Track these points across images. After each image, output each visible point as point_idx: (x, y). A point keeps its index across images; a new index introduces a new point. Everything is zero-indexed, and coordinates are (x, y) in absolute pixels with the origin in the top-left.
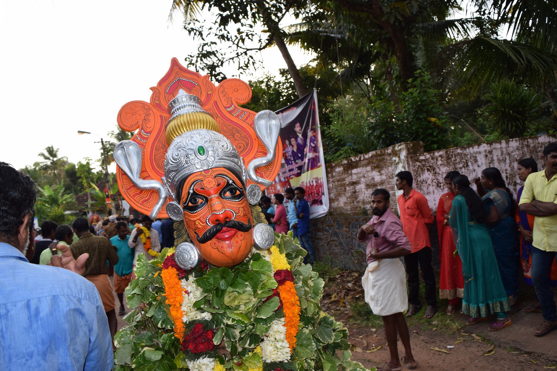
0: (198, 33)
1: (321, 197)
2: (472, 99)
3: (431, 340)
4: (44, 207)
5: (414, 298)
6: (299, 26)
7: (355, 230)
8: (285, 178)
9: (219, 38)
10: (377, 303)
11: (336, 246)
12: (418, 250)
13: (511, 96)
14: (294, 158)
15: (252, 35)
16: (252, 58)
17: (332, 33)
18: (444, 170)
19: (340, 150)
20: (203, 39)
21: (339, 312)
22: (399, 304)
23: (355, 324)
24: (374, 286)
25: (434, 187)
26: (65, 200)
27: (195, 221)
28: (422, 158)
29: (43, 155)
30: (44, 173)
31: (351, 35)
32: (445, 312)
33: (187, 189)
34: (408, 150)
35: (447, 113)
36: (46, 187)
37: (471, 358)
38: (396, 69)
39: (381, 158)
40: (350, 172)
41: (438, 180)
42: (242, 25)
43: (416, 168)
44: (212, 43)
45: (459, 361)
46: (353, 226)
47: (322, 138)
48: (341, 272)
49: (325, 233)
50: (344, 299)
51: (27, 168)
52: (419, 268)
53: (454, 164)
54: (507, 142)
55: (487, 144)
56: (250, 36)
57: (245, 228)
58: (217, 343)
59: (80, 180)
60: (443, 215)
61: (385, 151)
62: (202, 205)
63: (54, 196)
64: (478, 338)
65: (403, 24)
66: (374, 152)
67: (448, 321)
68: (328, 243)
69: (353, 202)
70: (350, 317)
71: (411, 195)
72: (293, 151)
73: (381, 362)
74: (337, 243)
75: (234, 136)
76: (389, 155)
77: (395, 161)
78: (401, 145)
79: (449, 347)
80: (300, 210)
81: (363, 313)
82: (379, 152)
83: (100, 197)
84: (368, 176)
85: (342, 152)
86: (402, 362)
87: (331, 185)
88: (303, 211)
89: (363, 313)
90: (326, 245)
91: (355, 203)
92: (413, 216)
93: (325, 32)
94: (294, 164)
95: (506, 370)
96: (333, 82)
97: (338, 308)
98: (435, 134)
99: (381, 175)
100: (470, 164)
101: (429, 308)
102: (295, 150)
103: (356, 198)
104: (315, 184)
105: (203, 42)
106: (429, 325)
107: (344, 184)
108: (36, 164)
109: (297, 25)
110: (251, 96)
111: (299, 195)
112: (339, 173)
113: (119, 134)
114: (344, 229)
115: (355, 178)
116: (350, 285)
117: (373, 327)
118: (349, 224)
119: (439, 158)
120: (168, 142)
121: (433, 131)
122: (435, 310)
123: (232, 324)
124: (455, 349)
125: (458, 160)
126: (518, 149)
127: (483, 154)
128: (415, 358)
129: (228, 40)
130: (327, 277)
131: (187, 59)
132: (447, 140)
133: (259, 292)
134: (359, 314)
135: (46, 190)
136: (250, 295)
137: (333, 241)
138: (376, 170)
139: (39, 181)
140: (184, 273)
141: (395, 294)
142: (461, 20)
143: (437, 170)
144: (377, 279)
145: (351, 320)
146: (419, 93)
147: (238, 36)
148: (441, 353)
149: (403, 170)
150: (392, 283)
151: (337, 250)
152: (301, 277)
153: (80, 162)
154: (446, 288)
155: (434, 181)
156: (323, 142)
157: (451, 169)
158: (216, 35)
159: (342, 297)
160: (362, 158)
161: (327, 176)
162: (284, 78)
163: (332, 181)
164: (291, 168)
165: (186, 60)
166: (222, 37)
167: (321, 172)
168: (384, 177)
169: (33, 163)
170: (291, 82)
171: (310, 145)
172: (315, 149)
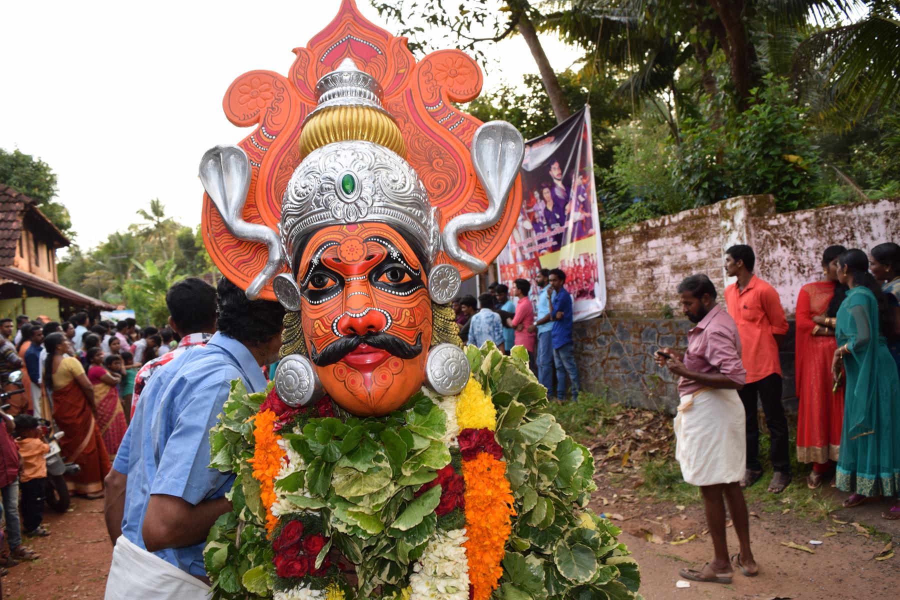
0: (393, 13)
1: (593, 285)
2: (849, 127)
3: (782, 529)
4: (145, 295)
7: (650, 342)
8: (531, 254)
9: (428, 20)
10: (689, 464)
11: (617, 368)
12: (758, 379)
14: (547, 221)
15: (483, 15)
16: (482, 54)
17: (612, 15)
19: (629, 207)
20: (402, 22)
21: (621, 476)
22: (730, 468)
23: (649, 496)
24: (686, 436)
25: (793, 273)
28: (773, 222)
29: (143, 213)
30: (143, 242)
31: (648, 16)
32: (804, 482)
34: (749, 208)
37: (852, 563)
39: (699, 222)
40: (644, 245)
41: (799, 260)
43: (761, 240)
44: (417, 29)
45: (832, 567)
46: (647, 335)
47: (597, 189)
48: (623, 411)
49: (599, 346)
50: (630, 454)
51: (118, 233)
52: (760, 408)
53: (830, 234)
55: (890, 201)
56: (480, 18)
57: (407, 351)
59: (200, 253)
60: (811, 318)
61: (707, 210)
63: (159, 278)
64: (863, 529)
67: (810, 499)
68: (603, 363)
69: (648, 296)
70: (640, 485)
71: (750, 285)
72: (546, 210)
73: (696, 561)
74: (618, 363)
75: (431, 163)
76: (715, 217)
77: (725, 227)
78: (736, 200)
79: (812, 542)
80: (556, 307)
81: (662, 479)
82: (696, 212)
84: (676, 253)
85: (632, 211)
86: (733, 563)
87: (610, 267)
88: (563, 308)
89: (662, 479)
90: (599, 364)
91: (652, 298)
92: (753, 321)
93: (601, 12)
94: (547, 230)
96: (612, 97)
97: (620, 470)
98: (795, 182)
100: (857, 234)
101: (776, 475)
102: (550, 208)
103: (654, 288)
104: (583, 264)
106: (775, 503)
107: (634, 265)
108: (133, 227)
111: (556, 283)
112: (626, 247)
114: (632, 339)
115: (652, 255)
116: (639, 432)
117: (679, 502)
118: (641, 332)
119: (804, 224)
121: (793, 178)
122: (786, 479)
124: (824, 546)
125: (837, 228)
127: (882, 218)
128: (755, 559)
129: (444, 23)
130: (602, 417)
132: (815, 194)
134: (656, 480)
135: (148, 268)
137: (611, 359)
138: (691, 242)
139: (136, 253)
143: (799, 244)
144: (689, 424)
145: (642, 490)
146: (770, 113)
147: (461, 18)
148: (799, 552)
149: (739, 243)
150: (712, 433)
151: (618, 374)
154: (815, 445)
156: (598, 195)
158: (424, 16)
159: (627, 451)
160: (667, 223)
161: (604, 252)
162: (531, 89)
163: (614, 260)
164: (541, 238)
166: (434, 19)
167: (593, 244)
168: (704, 255)
169: (128, 226)
170: (542, 97)
171: (577, 200)
172: (585, 206)
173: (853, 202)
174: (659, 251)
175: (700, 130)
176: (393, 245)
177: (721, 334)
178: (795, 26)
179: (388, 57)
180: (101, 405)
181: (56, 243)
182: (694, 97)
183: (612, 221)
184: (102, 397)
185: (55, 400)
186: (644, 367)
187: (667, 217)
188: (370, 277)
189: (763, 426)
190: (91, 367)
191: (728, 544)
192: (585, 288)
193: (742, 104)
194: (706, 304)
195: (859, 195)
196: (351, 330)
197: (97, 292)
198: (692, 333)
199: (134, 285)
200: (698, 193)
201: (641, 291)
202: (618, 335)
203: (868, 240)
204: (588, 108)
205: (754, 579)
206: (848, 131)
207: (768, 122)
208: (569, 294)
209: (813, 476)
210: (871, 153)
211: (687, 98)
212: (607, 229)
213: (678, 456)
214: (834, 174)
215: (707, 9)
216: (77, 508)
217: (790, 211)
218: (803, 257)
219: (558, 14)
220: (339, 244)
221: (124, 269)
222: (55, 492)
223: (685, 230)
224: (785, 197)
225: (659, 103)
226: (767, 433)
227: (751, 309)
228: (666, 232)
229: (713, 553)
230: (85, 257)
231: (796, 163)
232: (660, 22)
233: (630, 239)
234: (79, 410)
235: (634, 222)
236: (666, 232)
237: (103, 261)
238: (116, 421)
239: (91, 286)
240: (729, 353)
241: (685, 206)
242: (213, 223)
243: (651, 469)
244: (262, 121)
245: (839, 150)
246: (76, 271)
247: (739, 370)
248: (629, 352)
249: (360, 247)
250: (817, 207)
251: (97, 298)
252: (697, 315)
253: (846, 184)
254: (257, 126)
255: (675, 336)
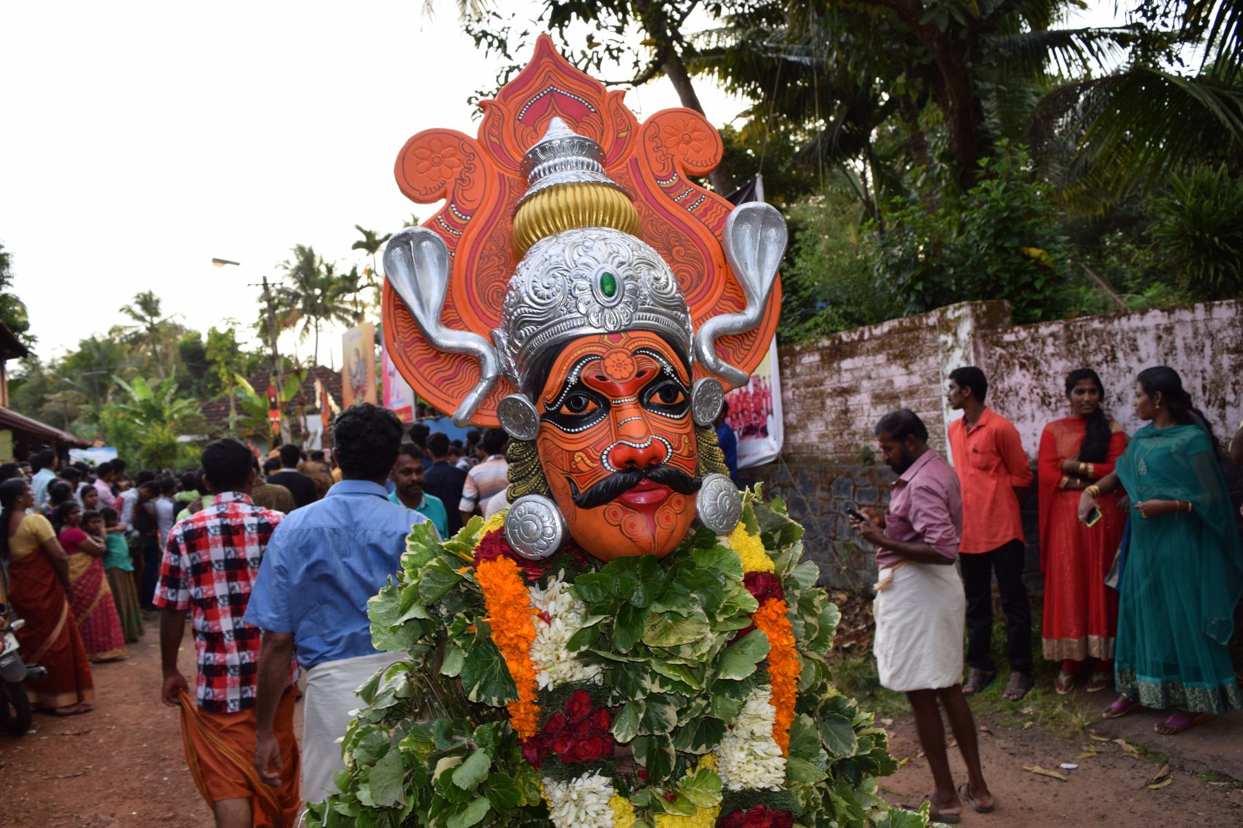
0: (496, 43)
1: (765, 419)
2: (1101, 211)
3: (1023, 749)
4: (133, 426)
5: (978, 653)
6: (715, 36)
7: (843, 496)
12: (994, 547)
13: (1216, 204)
15: (619, 50)
17: (790, 53)
18: (1059, 368)
20: (509, 57)
25: (1035, 406)
26: (177, 412)
27: (572, 453)
28: (1009, 337)
30: (129, 352)
32: (1050, 687)
33: (561, 374)
34: (977, 319)
35: (1066, 238)
36: (138, 381)
37: (1117, 794)
38: (938, 138)
39: (910, 335)
40: (835, 365)
41: (1044, 388)
42: (599, 27)
43: (993, 361)
45: (1091, 799)
46: (838, 488)
51: (93, 339)
52: (994, 585)
53: (1084, 354)
54: (1209, 309)
55: (1162, 311)
56: (615, 53)
58: (625, 737)
59: (213, 369)
62: (593, 416)
63: (153, 402)
64: (1131, 748)
65: (963, 35)
66: (895, 323)
67: (1059, 708)
69: (841, 434)
71: (981, 421)
73: (910, 793)
75: (670, 251)
76: (932, 329)
77: (946, 343)
78: (960, 307)
79: (1064, 766)
82: (906, 322)
83: (256, 407)
84: (879, 377)
85: (820, 320)
87: (789, 394)
91: (846, 437)
92: (985, 469)
95: (1202, 822)
96: (788, 164)
99: (910, 373)
100: (1120, 355)
101: (1015, 676)
103: (848, 424)
105: (507, 63)
107: (822, 393)
109: (710, 33)
110: (719, 158)
113: (299, 269)
114: (818, 493)
115: (846, 380)
118: (830, 483)
119: (1050, 340)
120: (517, 251)
121: (1034, 279)
122: (1028, 682)
123: (662, 691)
126: (1232, 324)
128: (989, 788)
131: (473, 100)
133: (720, 619)
135: (138, 388)
136: (702, 623)
138: (898, 362)
139: (120, 367)
140: (536, 571)
141: (922, 647)
142: (1086, 30)
143: (1044, 367)
146: (1005, 191)
148: (1047, 779)
149: (963, 364)
150: (915, 621)
152: (797, 593)
153: (214, 329)
154: (1068, 636)
155: (1036, 391)
157: (1076, 364)
160: (866, 336)
161: (781, 374)
163: (794, 386)
165: (469, 101)
168: (916, 380)
173: (1108, 313)
174: (856, 374)
175: (912, 212)
176: (665, 359)
177: (928, 490)
178: (1031, 76)
179: (604, 117)
180: (79, 583)
181: (7, 351)
182: (897, 167)
183: (792, 332)
184: (82, 571)
185: (12, 575)
186: (835, 531)
187: (866, 328)
188: (640, 398)
189: (998, 612)
190: (63, 529)
191: (952, 770)
192: (754, 423)
193: (965, 178)
194: (911, 449)
195: (1115, 301)
196: (630, 465)
197: (63, 422)
198: (894, 487)
199: (117, 413)
200: (909, 296)
201: (830, 428)
202: (799, 488)
203: (1134, 363)
204: (759, 178)
205: (989, 817)
206: (1100, 216)
207: (1003, 204)
208: (732, 430)
209: (1063, 678)
210: (1129, 246)
211: (890, 168)
212: (785, 343)
213: (876, 652)
214: (1081, 273)
215: (919, 51)
216: (41, 729)
217: (1031, 322)
218: (1049, 384)
219: (718, 50)
220: (602, 358)
221: (103, 389)
222: (11, 706)
223: (891, 347)
224: (1024, 304)
225: (850, 173)
226: (1003, 620)
227: (982, 453)
228: (865, 349)
229: (933, 782)
230: (47, 372)
231: (1038, 259)
232: (856, 67)
233: (816, 358)
234: (47, 589)
235: (823, 334)
236: (865, 349)
237: (71, 378)
238: (101, 605)
239: (54, 413)
240: (936, 515)
241: (892, 314)
242: (400, 329)
243: (846, 669)
244: (450, 195)
245: (1088, 240)
246: (32, 392)
247: (948, 540)
248: (814, 510)
249: (629, 361)
250: (1066, 318)
251: (63, 429)
252: (902, 463)
253: (1097, 286)
254: (442, 203)
255: (877, 489)
